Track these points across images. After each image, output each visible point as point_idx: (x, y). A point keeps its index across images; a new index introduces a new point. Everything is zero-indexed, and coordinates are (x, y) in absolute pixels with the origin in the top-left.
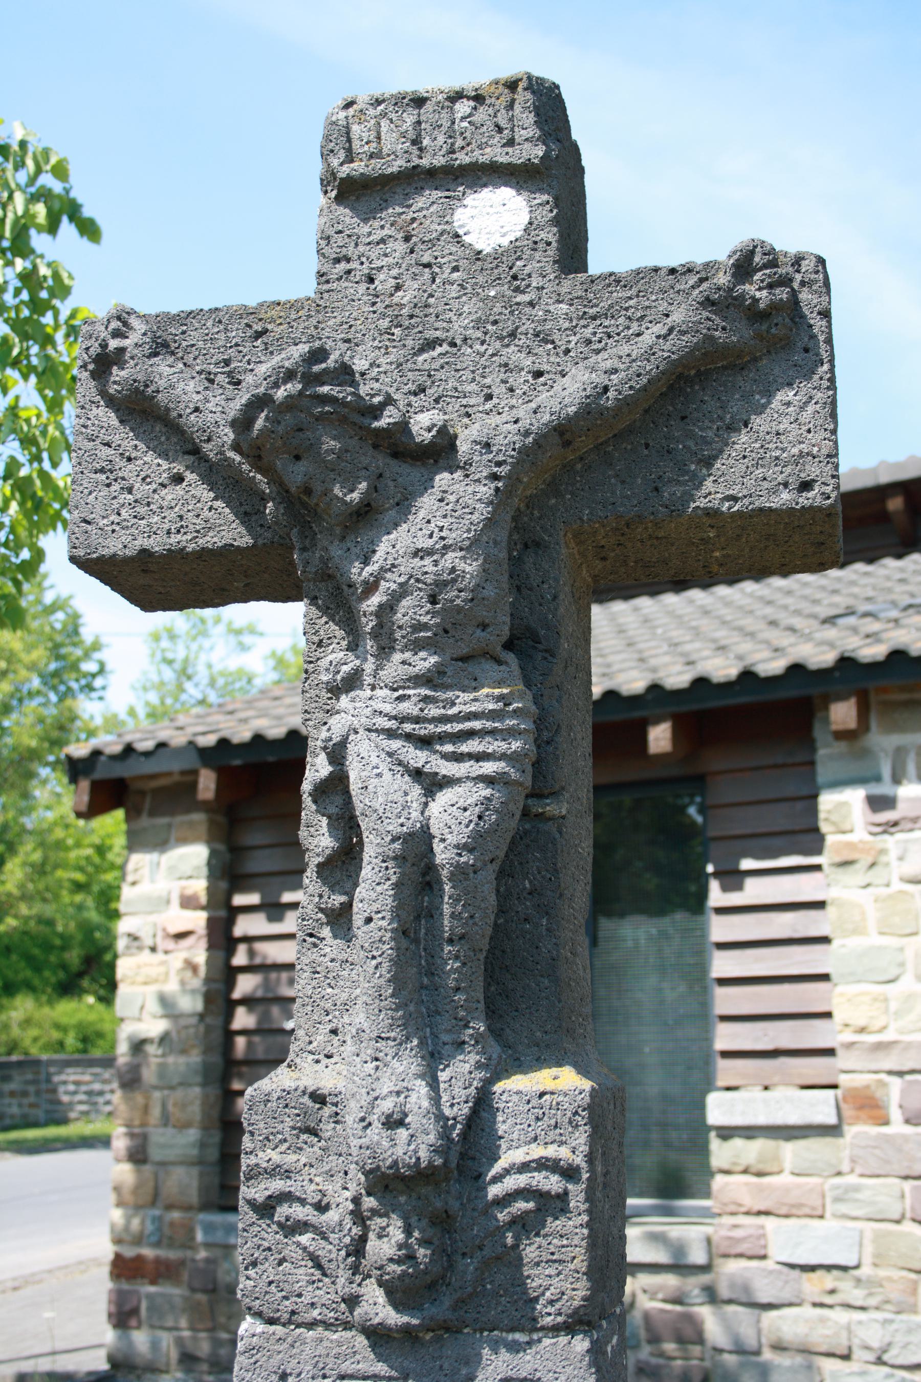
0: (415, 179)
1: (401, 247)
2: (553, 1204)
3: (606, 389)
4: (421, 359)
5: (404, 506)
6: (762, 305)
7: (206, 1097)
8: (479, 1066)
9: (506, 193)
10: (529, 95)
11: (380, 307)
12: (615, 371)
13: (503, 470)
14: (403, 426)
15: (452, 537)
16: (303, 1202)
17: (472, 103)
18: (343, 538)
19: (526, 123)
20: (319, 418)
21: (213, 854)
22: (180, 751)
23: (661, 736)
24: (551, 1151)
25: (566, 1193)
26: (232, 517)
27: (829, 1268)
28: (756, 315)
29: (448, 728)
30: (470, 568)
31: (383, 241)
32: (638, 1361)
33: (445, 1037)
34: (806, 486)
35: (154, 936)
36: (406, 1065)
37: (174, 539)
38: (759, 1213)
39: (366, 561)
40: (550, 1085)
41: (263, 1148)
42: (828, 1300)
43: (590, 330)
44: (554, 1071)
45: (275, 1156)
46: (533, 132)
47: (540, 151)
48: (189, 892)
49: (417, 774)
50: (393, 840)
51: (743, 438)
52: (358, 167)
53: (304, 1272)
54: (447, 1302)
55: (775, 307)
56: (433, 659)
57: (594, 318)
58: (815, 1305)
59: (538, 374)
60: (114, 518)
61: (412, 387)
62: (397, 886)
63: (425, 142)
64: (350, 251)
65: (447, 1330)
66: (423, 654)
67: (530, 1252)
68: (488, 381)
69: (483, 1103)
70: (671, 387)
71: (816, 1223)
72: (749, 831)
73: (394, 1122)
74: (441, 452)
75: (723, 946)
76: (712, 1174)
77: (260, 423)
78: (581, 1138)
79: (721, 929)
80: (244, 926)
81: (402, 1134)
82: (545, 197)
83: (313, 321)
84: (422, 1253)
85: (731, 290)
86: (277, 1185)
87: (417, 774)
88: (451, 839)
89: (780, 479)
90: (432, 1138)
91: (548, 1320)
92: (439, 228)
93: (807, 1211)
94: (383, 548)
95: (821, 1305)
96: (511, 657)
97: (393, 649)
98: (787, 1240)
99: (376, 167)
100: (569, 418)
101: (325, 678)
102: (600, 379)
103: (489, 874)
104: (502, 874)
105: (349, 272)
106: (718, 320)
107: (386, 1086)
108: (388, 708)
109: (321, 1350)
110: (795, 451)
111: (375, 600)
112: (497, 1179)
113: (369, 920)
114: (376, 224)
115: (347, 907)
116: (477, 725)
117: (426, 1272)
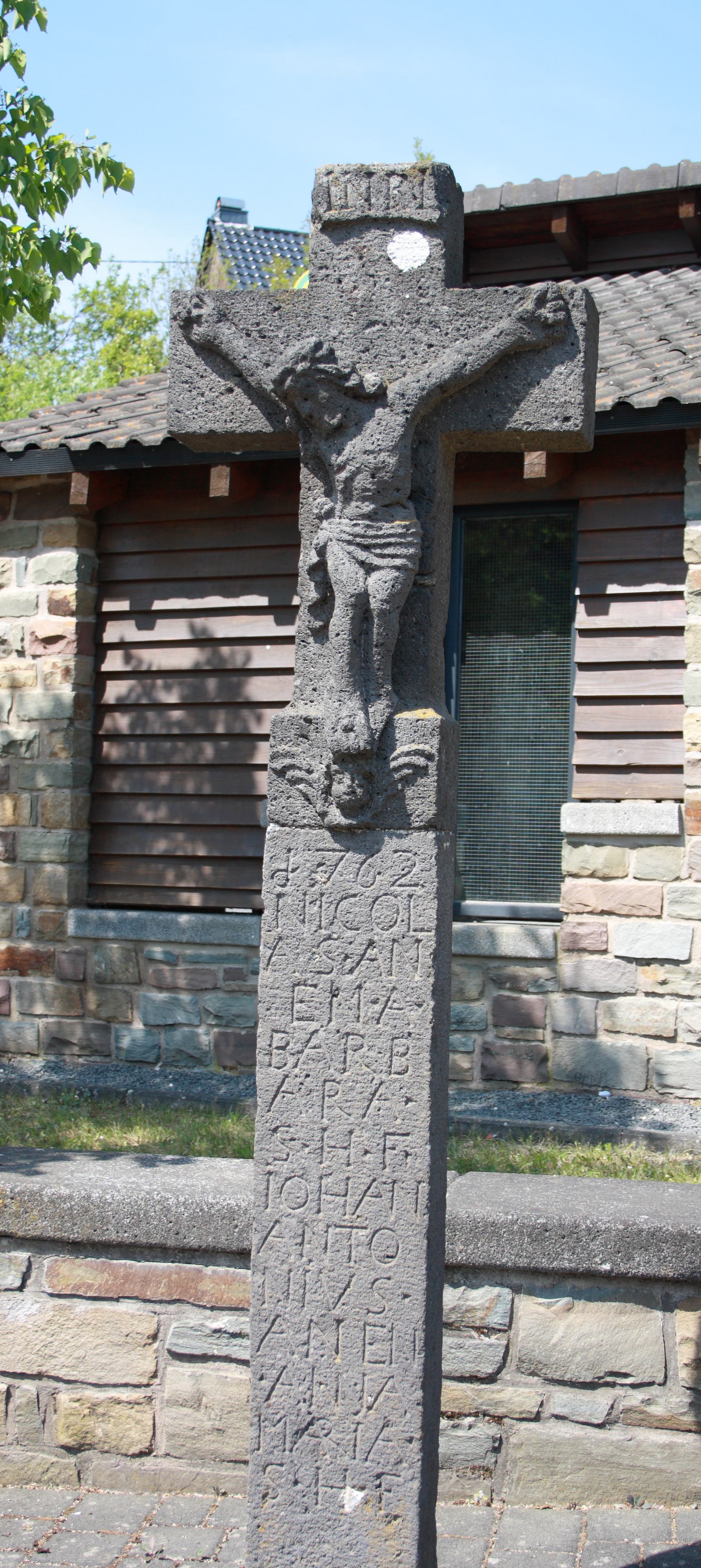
0: (366, 223)
1: (357, 263)
2: (420, 771)
3: (465, 364)
4: (367, 331)
5: (359, 427)
6: (550, 321)
7: (75, 799)
8: (388, 706)
9: (417, 236)
10: (432, 179)
11: (345, 299)
12: (471, 354)
13: (410, 409)
14: (361, 385)
15: (384, 445)
16: (300, 769)
17: (400, 179)
18: (327, 439)
19: (430, 197)
20: (319, 380)
21: (82, 559)
22: (50, 453)
23: (536, 461)
24: (421, 747)
25: (427, 766)
26: (261, 415)
27: (663, 962)
28: (546, 325)
29: (378, 541)
30: (392, 461)
31: (347, 258)
32: (485, 1043)
33: (372, 692)
34: (567, 419)
35: (22, 640)
36: (354, 703)
37: (229, 425)
38: (603, 913)
39: (339, 453)
40: (421, 716)
41: (280, 744)
42: (660, 990)
43: (460, 323)
44: (424, 710)
45: (286, 748)
46: (434, 202)
47: (436, 215)
48: (58, 597)
49: (362, 564)
50: (352, 596)
51: (536, 391)
52: (333, 214)
53: (300, 802)
54: (369, 815)
55: (556, 323)
56: (372, 506)
57: (462, 316)
58: (647, 994)
59: (430, 346)
60: (193, 410)
61: (361, 348)
62: (352, 619)
63: (373, 200)
64: (328, 262)
65: (369, 828)
66: (367, 503)
67: (409, 793)
68: (403, 348)
69: (389, 724)
70: (500, 360)
71: (654, 921)
72: (617, 558)
73: (348, 729)
74: (379, 397)
75: (585, 667)
76: (562, 878)
77: (288, 382)
78: (435, 741)
79: (585, 650)
80: (112, 633)
81: (352, 735)
82: (439, 241)
83: (307, 304)
84: (359, 791)
85: (534, 313)
86: (287, 761)
87: (362, 564)
88: (379, 597)
89: (554, 414)
90: (366, 737)
91: (416, 824)
92: (379, 254)
93: (647, 911)
94: (348, 448)
95: (654, 994)
96: (410, 505)
97: (351, 499)
98: (627, 937)
99: (345, 214)
100: (445, 381)
101: (316, 511)
102: (460, 358)
103: (396, 614)
104: (402, 614)
105: (327, 276)
106: (526, 329)
107: (344, 713)
108: (348, 529)
109: (308, 838)
110: (562, 400)
111: (343, 475)
112: (395, 759)
113: (338, 635)
114: (343, 247)
115: (325, 627)
116: (393, 540)
117: (360, 800)
